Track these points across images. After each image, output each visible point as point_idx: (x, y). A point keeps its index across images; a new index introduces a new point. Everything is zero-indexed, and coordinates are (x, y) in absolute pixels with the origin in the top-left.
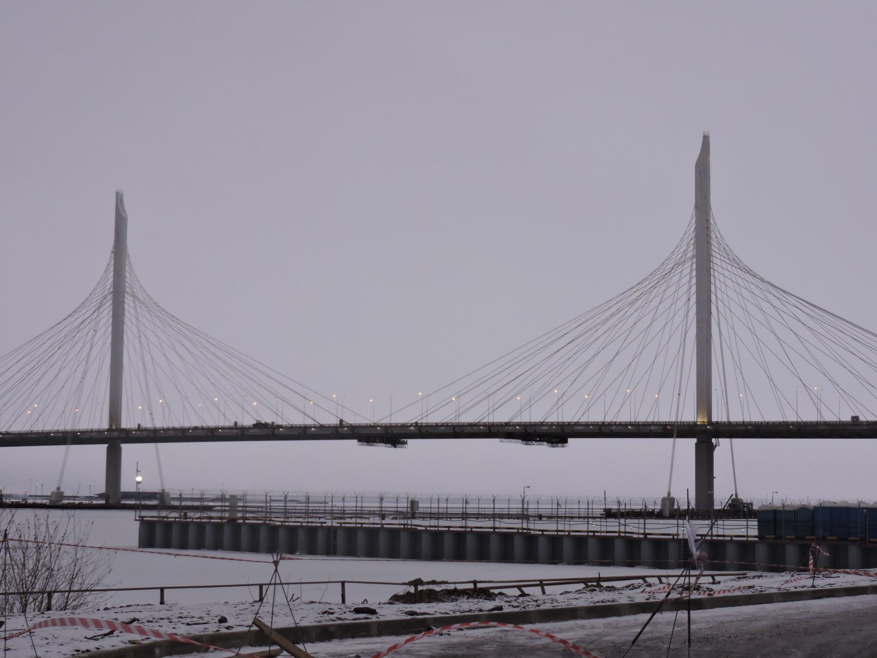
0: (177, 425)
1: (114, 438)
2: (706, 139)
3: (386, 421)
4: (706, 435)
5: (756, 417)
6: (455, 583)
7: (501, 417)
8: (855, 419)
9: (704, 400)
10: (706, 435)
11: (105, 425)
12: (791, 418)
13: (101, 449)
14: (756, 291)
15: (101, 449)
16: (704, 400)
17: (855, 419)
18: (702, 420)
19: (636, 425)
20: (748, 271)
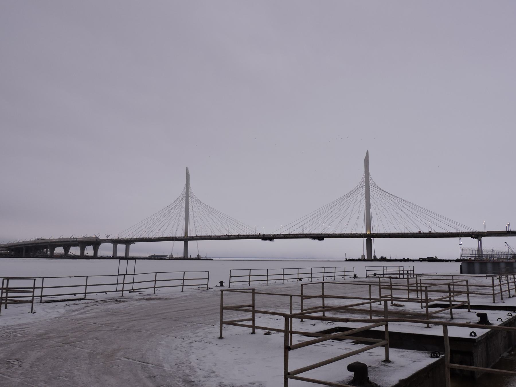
0: (209, 235)
1: (186, 239)
2: (367, 151)
3: (274, 233)
4: (369, 237)
5: (389, 232)
6: (478, 236)
7: (305, 232)
8: (420, 232)
9: (369, 226)
10: (369, 237)
11: (183, 235)
12: (400, 232)
13: (182, 242)
14: (387, 197)
15: (182, 242)
16: (369, 226)
17: (420, 232)
18: (368, 233)
19: (402, 234)
20: (381, 189)
